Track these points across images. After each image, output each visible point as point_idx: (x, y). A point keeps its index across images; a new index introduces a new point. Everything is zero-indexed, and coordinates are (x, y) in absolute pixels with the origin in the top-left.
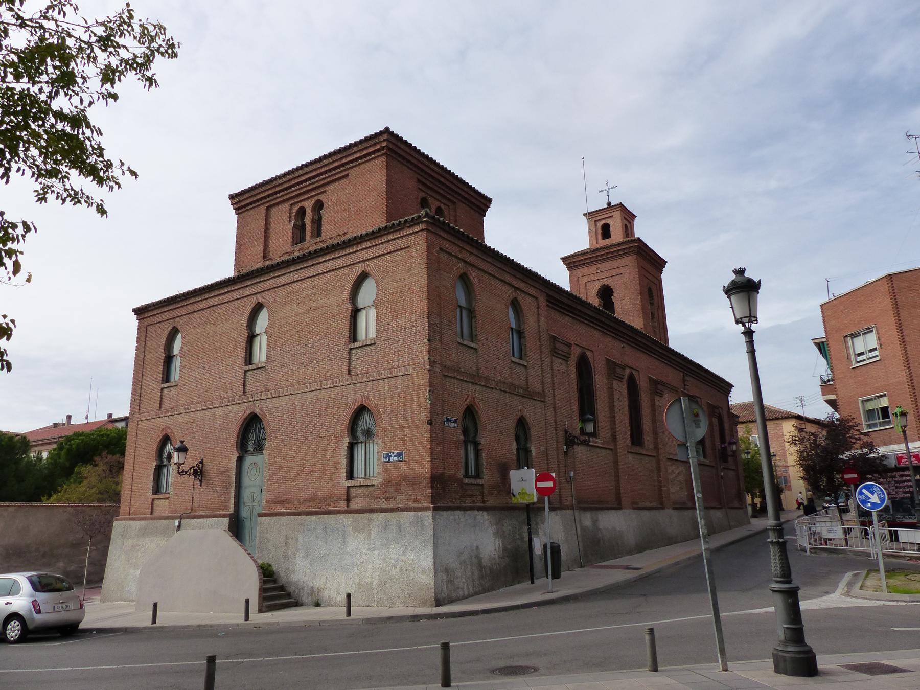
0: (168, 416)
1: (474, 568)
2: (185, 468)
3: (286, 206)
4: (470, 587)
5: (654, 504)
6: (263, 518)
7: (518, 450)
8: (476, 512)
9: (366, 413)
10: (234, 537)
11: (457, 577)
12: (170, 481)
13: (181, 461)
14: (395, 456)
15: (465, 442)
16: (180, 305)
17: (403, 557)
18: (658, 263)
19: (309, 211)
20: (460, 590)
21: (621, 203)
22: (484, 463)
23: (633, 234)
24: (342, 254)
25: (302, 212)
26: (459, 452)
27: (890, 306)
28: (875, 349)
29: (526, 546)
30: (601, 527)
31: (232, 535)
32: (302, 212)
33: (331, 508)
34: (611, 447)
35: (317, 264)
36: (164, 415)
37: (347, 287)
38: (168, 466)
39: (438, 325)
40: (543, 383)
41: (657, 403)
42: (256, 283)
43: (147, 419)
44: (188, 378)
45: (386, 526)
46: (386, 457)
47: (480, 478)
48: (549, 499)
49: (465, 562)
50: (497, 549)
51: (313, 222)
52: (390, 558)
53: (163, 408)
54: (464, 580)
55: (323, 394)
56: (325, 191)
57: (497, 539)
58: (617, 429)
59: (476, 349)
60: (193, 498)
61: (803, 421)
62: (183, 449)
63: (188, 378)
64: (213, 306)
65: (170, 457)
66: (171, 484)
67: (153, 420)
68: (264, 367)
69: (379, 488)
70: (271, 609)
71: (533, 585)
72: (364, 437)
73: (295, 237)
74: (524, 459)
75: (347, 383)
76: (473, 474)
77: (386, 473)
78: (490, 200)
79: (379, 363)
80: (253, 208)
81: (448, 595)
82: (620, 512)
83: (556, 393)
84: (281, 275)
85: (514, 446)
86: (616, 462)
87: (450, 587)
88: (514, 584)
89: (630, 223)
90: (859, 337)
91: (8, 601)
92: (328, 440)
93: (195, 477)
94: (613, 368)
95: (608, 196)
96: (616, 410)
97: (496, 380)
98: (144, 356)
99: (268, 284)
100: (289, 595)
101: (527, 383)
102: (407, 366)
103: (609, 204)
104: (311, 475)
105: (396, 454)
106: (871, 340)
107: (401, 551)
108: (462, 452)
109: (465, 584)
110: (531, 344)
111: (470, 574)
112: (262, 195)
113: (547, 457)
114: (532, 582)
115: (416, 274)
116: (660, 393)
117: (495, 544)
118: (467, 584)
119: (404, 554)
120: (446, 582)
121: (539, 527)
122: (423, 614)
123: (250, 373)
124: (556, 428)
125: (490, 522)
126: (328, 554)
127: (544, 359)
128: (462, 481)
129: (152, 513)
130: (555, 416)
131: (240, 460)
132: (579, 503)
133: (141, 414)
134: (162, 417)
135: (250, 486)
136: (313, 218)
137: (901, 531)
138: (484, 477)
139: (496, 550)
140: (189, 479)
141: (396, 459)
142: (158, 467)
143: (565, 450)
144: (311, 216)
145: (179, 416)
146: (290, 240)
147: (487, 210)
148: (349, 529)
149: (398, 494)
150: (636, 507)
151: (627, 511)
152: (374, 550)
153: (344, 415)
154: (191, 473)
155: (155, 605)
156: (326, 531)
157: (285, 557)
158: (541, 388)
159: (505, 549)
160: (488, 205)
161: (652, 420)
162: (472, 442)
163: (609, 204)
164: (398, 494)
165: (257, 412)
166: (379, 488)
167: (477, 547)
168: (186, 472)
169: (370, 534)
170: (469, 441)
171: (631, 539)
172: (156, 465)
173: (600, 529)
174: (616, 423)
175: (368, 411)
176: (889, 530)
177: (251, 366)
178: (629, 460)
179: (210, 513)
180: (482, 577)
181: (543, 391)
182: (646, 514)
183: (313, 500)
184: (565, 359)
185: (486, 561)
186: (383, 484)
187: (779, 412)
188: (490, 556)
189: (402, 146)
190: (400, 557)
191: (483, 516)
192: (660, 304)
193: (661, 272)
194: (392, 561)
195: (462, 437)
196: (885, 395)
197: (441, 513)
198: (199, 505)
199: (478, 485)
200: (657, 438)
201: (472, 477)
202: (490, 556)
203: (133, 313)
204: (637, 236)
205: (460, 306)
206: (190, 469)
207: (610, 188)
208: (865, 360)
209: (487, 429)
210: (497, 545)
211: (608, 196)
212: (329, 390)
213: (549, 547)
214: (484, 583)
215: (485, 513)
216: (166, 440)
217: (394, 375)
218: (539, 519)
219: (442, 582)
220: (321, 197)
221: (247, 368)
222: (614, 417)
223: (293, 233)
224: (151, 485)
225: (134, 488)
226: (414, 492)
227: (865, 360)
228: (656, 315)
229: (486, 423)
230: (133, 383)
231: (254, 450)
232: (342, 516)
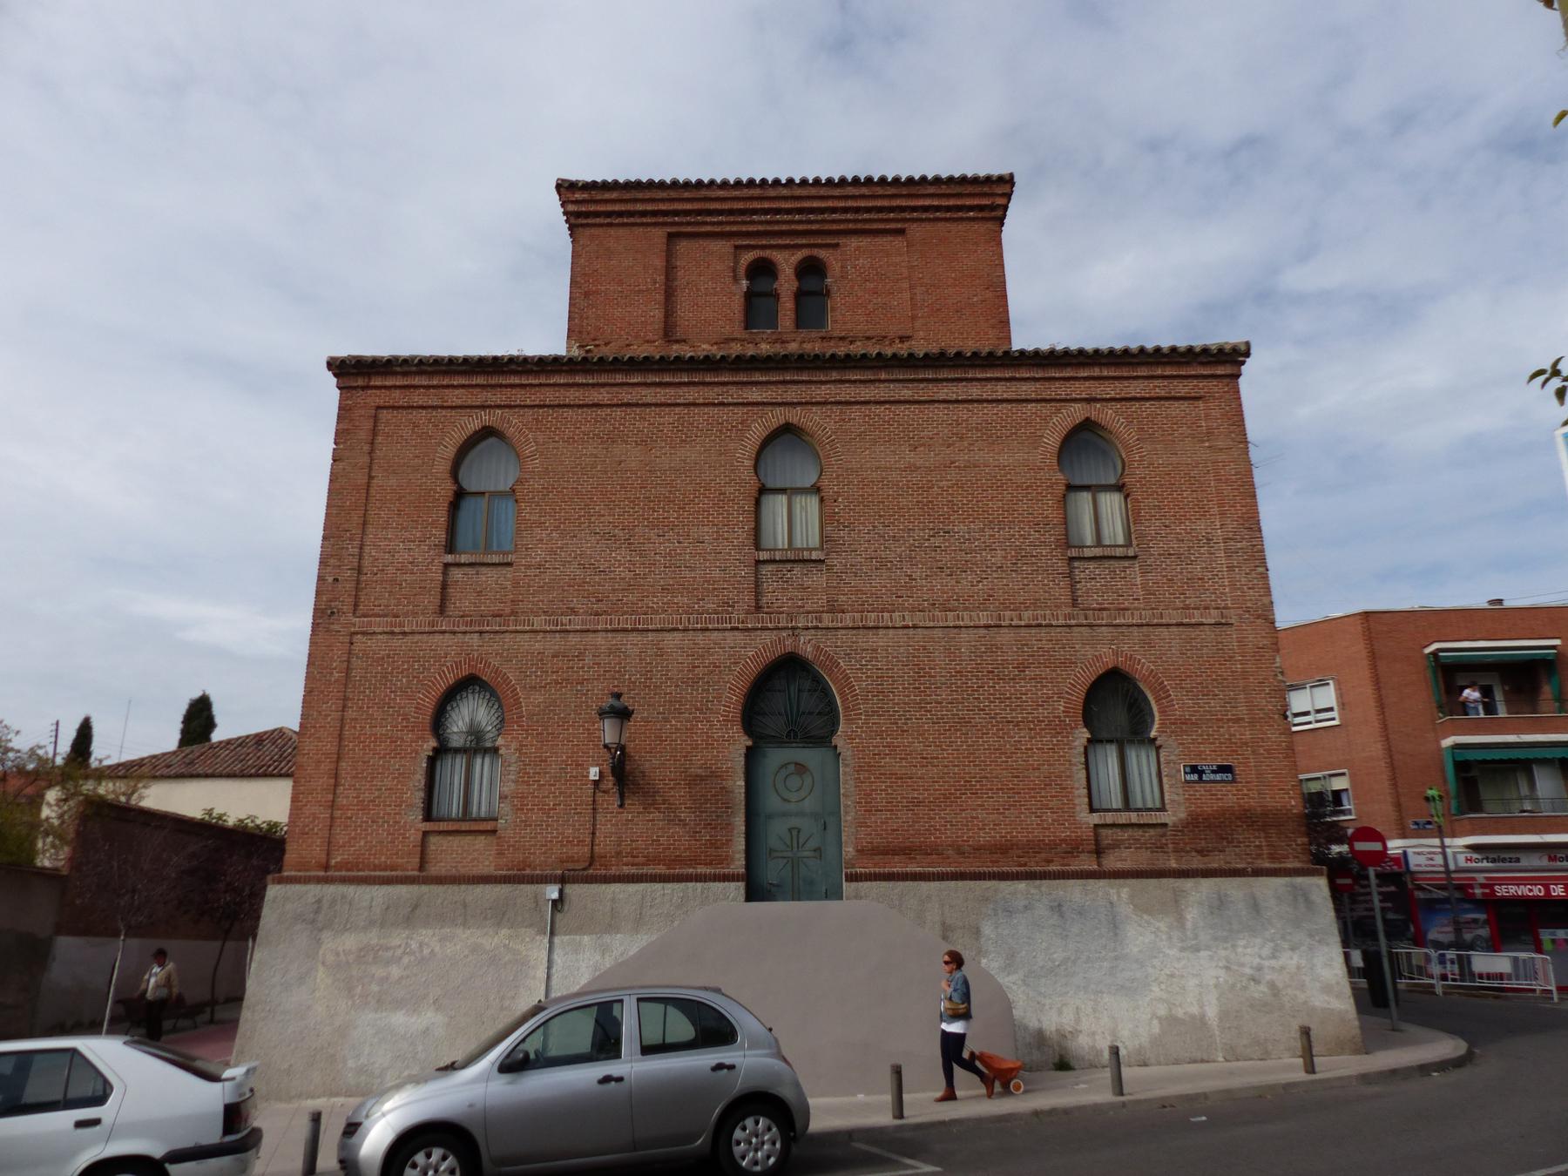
0: (481, 633)
6: (861, 884)
14: (1214, 772)
16: (515, 380)
17: (1273, 963)
24: (1037, 376)
27: (1364, 653)
28: (1331, 709)
33: (1053, 868)
35: (967, 380)
36: (463, 628)
42: (784, 382)
43: (392, 633)
45: (1220, 904)
52: (1242, 965)
53: (450, 608)
55: (1005, 637)
56: (837, 245)
64: (637, 405)
67: (417, 637)
69: (1180, 831)
75: (1073, 622)
80: (642, 224)
84: (861, 381)
90: (1304, 690)
91: (717, 1061)
92: (1031, 729)
98: (371, 478)
99: (821, 392)
105: (1215, 768)
106: (1327, 696)
107: (1266, 951)
112: (662, 207)
115: (1222, 449)
119: (1274, 957)
122: (1437, 1060)
129: (421, 868)
134: (454, 633)
135: (785, 815)
137: (1476, 957)
141: (1212, 777)
145: (527, 636)
148: (1125, 909)
152: (1198, 950)
153: (1070, 683)
155: (897, 1072)
166: (1180, 831)
169: (1181, 919)
176: (1457, 955)
179: (661, 869)
186: (1188, 823)
190: (1266, 963)
194: (1248, 971)
196: (1343, 774)
208: (1310, 723)
212: (1023, 630)
217: (1193, 621)
221: (449, 558)
225: (341, 801)
227: (1310, 723)
231: (788, 735)
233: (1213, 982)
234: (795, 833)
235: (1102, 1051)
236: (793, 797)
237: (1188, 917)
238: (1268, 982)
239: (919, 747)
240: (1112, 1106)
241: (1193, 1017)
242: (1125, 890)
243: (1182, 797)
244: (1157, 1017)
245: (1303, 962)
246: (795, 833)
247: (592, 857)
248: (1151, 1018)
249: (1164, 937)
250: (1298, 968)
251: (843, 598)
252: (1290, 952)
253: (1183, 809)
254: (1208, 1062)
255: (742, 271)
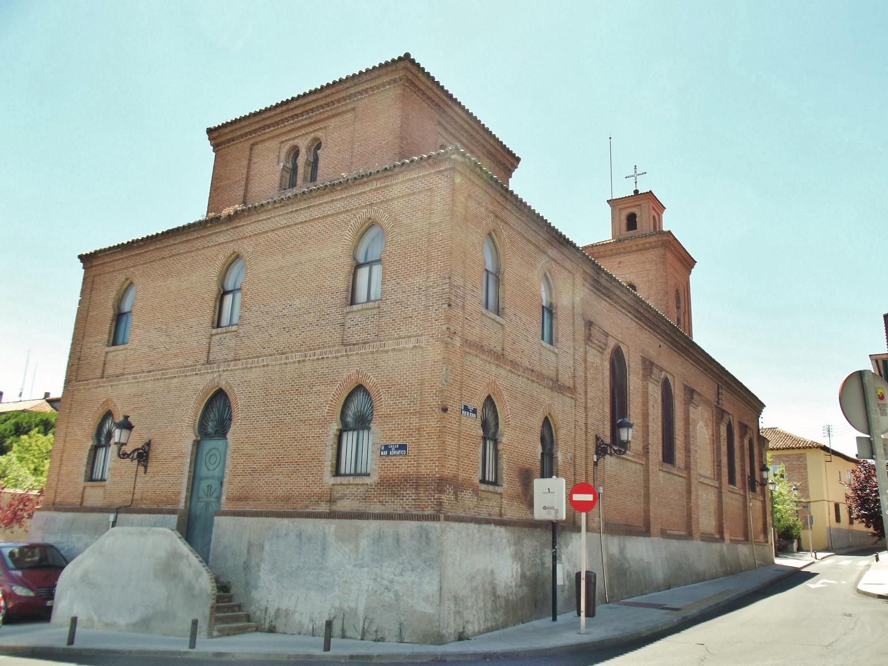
1: (488, 597)
2: (128, 449)
3: (274, 143)
4: (482, 623)
5: (683, 533)
7: (542, 454)
8: (492, 527)
9: (361, 394)
10: (183, 539)
11: (467, 608)
12: (108, 465)
13: (123, 441)
14: (396, 449)
15: (484, 439)
17: (400, 579)
18: (688, 263)
19: (303, 151)
20: (469, 625)
21: (651, 191)
22: (504, 467)
23: (660, 226)
25: (295, 152)
26: (477, 449)
29: (549, 573)
30: (628, 556)
31: (180, 535)
32: (295, 152)
34: (642, 462)
37: (347, 236)
38: (107, 445)
39: (461, 288)
40: (574, 377)
41: (692, 416)
44: (140, 341)
46: (385, 450)
47: (498, 486)
48: (587, 516)
49: (476, 588)
50: (515, 574)
51: (307, 164)
52: (383, 578)
54: (474, 612)
57: (515, 563)
58: (650, 442)
59: (502, 325)
60: (134, 488)
61: (829, 452)
62: (127, 425)
63: (140, 341)
65: (110, 435)
66: (109, 469)
68: (236, 331)
70: (224, 633)
71: (555, 623)
72: (357, 424)
73: (284, 181)
74: (548, 469)
76: (491, 480)
77: (383, 470)
78: (518, 160)
79: (382, 331)
81: (455, 630)
82: (647, 539)
83: (588, 391)
85: (539, 449)
86: (647, 480)
87: (458, 620)
88: (532, 620)
89: (659, 215)
93: (139, 461)
94: (648, 366)
95: (636, 183)
96: (651, 418)
97: (523, 365)
100: (248, 618)
101: (557, 375)
102: (419, 336)
103: (636, 192)
104: (286, 467)
107: (398, 571)
108: (480, 450)
109: (476, 617)
110: (563, 329)
111: (482, 604)
113: (575, 467)
114: (554, 619)
116: (696, 405)
117: (512, 569)
118: (479, 617)
119: (401, 575)
120: (454, 613)
121: (562, 551)
123: (218, 337)
124: (586, 432)
125: (509, 540)
126: (302, 569)
127: (577, 348)
128: (478, 486)
130: (586, 418)
131: (197, 444)
132: (606, 525)
133: (78, 381)
135: (207, 478)
136: (307, 159)
138: (504, 484)
139: (513, 576)
140: (130, 465)
142: (93, 448)
143: (596, 460)
144: (305, 157)
146: (277, 185)
147: (514, 171)
149: (397, 497)
150: (664, 534)
151: (656, 539)
152: (363, 567)
154: (135, 457)
156: (300, 538)
157: (247, 567)
158: (572, 382)
159: (523, 576)
160: (515, 164)
161: (685, 436)
162: (492, 440)
163: (636, 192)
164: (397, 497)
165: (223, 385)
167: (492, 571)
168: (129, 455)
170: (489, 439)
171: (659, 573)
172: (92, 446)
173: (626, 558)
174: (650, 434)
175: (364, 391)
177: (219, 329)
178: (660, 477)
180: (495, 610)
181: (574, 386)
182: (674, 543)
183: (287, 499)
184: (601, 350)
185: (501, 590)
186: (378, 483)
187: (798, 440)
188: (506, 584)
189: (424, 79)
191: (500, 532)
192: (687, 309)
193: (690, 272)
194: (385, 582)
195: (481, 432)
197: (452, 524)
198: (142, 498)
199: (496, 493)
200: (690, 457)
201: (489, 483)
202: (506, 584)
203: (79, 260)
204: (665, 228)
205: (486, 270)
206: (134, 451)
207: (639, 175)
209: (509, 424)
210: (515, 570)
211: (636, 183)
213: (583, 576)
214: (497, 617)
215: (503, 529)
216: (109, 414)
218: (563, 542)
219: (449, 613)
220: (319, 134)
221: (214, 331)
222: (647, 427)
223: (282, 177)
224: (83, 469)
225: (62, 472)
226: (418, 496)
228: (682, 320)
229: (509, 418)
230: (72, 344)
231: (215, 433)
232: (323, 521)
233: (366, 588)
234: (210, 487)
235: (304, 625)
236: (212, 467)
237: (361, 545)
238: (394, 591)
239: (260, 438)
240: (186, 653)
241: (351, 609)
242: (333, 526)
243: (378, 466)
244: (334, 608)
245: (417, 580)
246: (210, 487)
247: (132, 500)
248: (331, 608)
249: (347, 557)
250: (413, 583)
251: (241, 352)
252: (411, 573)
253: (377, 474)
254: (353, 639)
255: (283, 155)
